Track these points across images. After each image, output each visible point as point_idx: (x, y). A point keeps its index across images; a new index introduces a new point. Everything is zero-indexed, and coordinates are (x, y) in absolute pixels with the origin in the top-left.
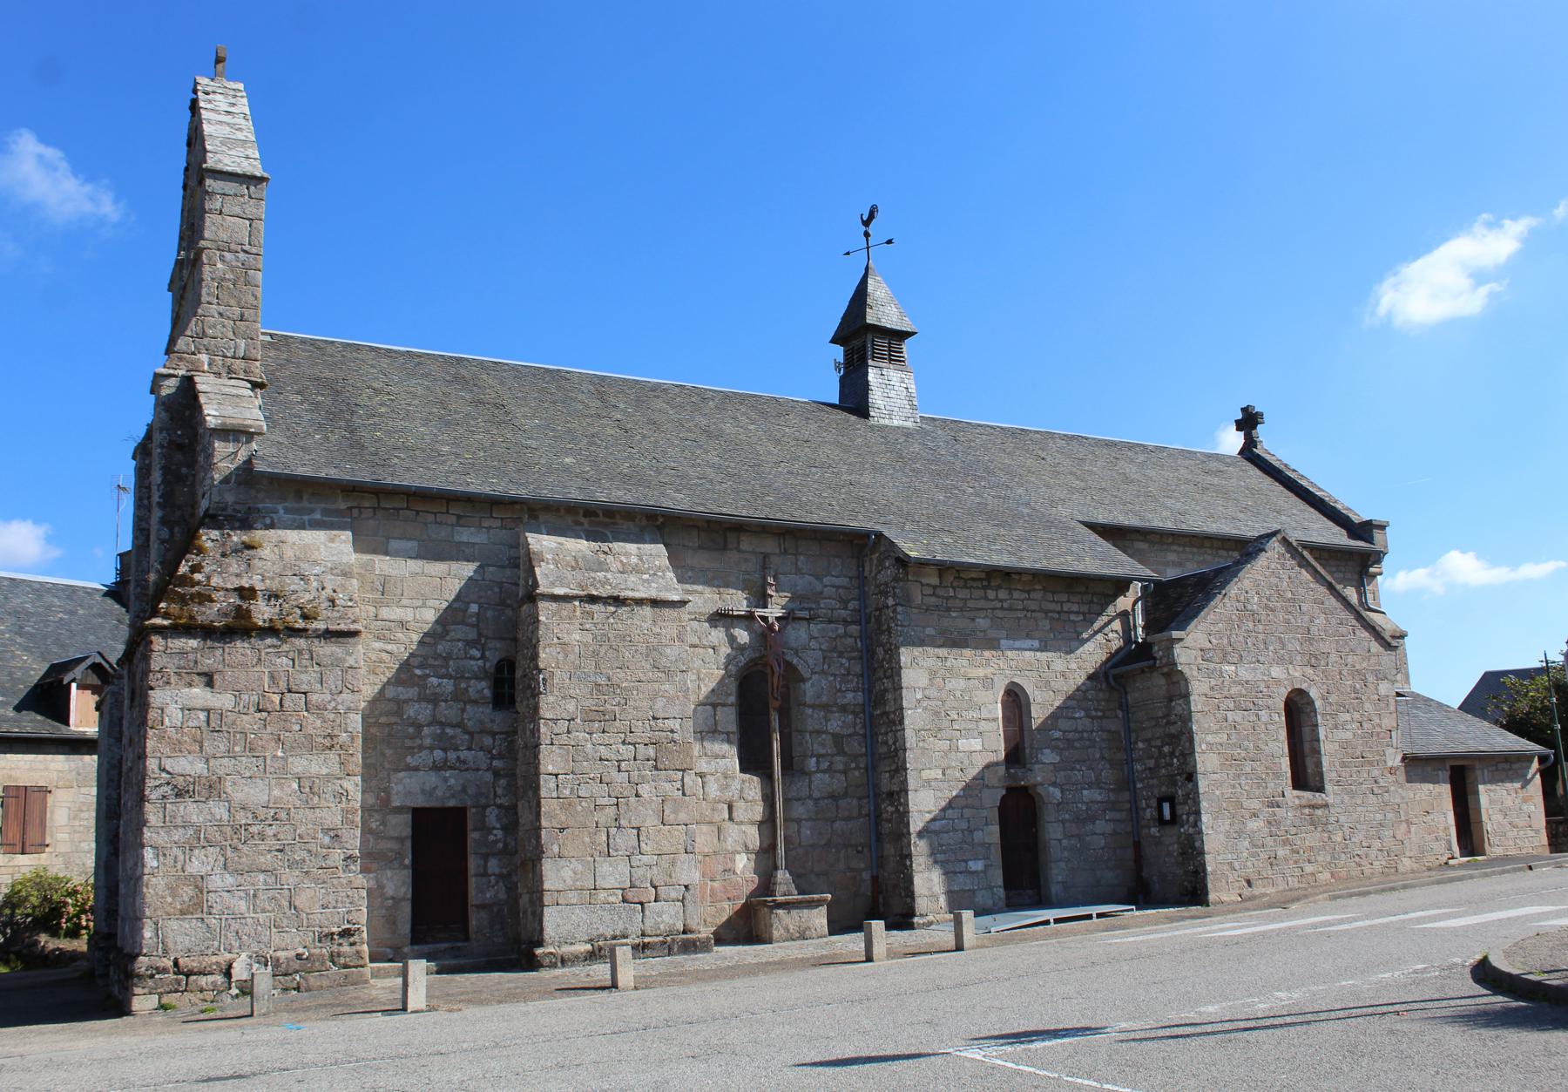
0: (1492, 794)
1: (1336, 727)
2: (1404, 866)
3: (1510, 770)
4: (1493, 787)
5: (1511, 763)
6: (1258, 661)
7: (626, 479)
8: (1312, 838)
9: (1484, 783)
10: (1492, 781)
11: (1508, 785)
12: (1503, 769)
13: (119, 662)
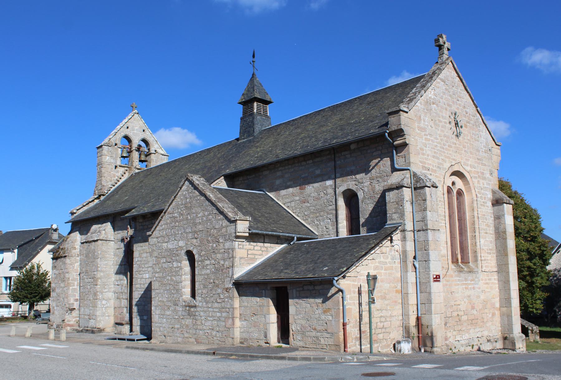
0: (298, 306)
1: (203, 268)
2: (229, 342)
3: (313, 290)
4: (300, 301)
5: (314, 285)
6: (175, 240)
7: (81, 335)
8: (189, 321)
9: (293, 298)
10: (299, 297)
11: (312, 300)
12: (308, 290)
13: (527, 350)
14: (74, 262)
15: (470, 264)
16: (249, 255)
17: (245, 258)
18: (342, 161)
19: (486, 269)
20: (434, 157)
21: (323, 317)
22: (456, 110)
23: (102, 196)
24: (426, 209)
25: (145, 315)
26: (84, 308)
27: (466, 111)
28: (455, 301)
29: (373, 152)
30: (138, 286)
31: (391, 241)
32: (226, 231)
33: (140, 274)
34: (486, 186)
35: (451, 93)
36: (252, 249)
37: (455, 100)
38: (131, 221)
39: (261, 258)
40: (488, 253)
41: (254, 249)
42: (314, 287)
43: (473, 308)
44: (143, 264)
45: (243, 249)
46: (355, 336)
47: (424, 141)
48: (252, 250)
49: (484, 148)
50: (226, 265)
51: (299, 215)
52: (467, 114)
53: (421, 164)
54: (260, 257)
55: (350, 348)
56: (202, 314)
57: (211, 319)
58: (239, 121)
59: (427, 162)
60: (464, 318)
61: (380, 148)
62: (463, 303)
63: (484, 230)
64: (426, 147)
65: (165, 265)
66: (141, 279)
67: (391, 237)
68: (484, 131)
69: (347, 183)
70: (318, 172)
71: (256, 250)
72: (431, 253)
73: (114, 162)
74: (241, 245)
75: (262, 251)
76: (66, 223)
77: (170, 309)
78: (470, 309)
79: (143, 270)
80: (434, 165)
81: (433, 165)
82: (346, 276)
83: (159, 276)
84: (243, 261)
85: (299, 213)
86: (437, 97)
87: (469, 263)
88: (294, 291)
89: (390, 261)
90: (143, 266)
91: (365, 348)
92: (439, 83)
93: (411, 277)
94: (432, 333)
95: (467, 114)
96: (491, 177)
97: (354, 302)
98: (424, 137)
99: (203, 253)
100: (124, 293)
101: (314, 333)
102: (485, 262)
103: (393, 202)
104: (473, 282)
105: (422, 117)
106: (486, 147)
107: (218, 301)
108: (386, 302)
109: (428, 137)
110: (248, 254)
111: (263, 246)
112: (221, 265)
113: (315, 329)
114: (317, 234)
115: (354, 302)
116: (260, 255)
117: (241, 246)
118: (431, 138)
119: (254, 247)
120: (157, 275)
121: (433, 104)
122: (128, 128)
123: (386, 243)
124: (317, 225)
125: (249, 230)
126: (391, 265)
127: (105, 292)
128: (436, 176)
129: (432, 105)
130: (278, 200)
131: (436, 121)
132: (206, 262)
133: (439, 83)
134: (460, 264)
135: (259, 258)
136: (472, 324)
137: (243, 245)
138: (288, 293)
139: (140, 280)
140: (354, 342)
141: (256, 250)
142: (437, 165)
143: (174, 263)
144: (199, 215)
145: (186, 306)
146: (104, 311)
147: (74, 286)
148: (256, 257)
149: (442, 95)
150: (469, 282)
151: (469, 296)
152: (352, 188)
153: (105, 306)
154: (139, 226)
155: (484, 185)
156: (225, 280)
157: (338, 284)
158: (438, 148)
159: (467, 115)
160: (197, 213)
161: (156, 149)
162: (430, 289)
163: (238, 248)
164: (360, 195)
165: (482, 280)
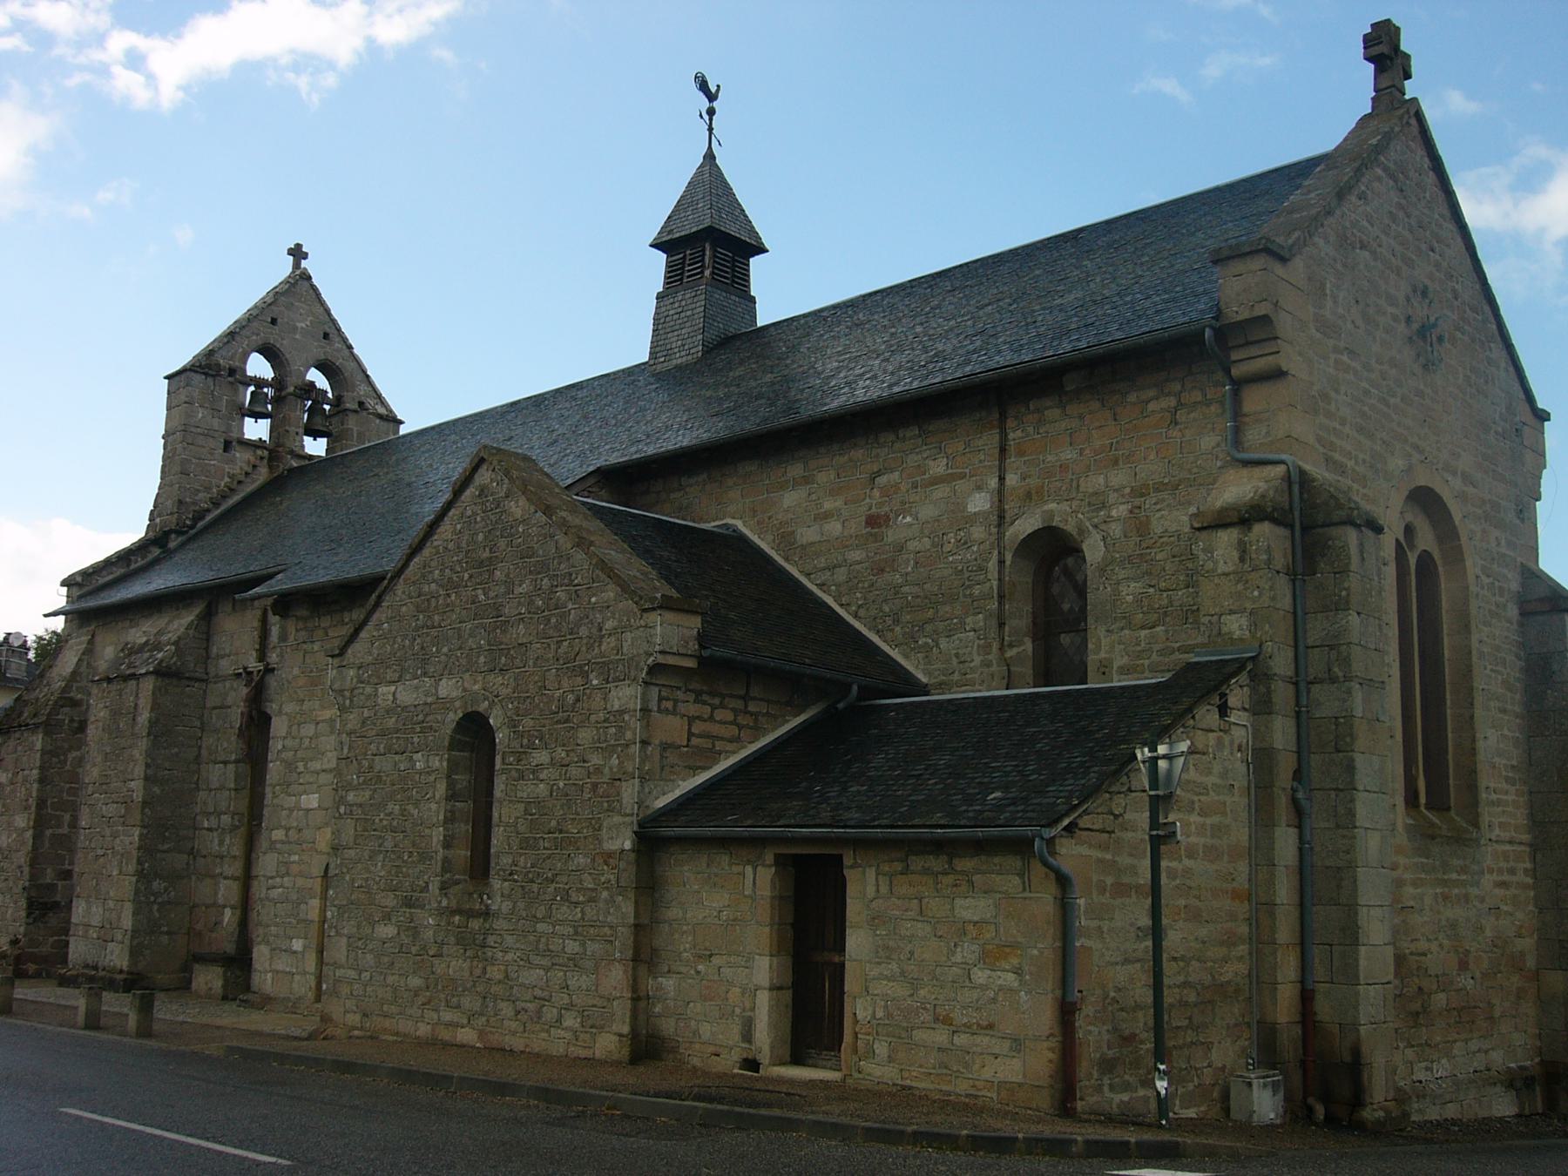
3: (945, 873)
8: (456, 966)
12: (926, 871)
14: (66, 746)
15: (1452, 813)
16: (693, 738)
17: (680, 747)
18: (1030, 429)
19: (1502, 834)
20: (1360, 430)
21: (980, 976)
22: (1427, 282)
23: (173, 536)
24: (1347, 602)
25: (298, 938)
26: (88, 902)
27: (1454, 291)
28: (1412, 941)
29: (1147, 402)
30: (278, 835)
31: (1223, 710)
32: (619, 650)
33: (290, 795)
34: (1503, 550)
35: (1413, 222)
36: (706, 716)
37: (1424, 247)
38: (270, 613)
39: (734, 752)
40: (1507, 779)
41: (711, 718)
42: (950, 863)
43: (1463, 966)
44: (303, 760)
45: (674, 713)
46: (1098, 1055)
47: (1331, 370)
48: (705, 721)
49: (1502, 423)
50: (611, 768)
51: (862, 613)
52: (1456, 299)
53: (1321, 449)
54: (730, 747)
55: (1082, 1099)
56: (509, 940)
57: (545, 962)
58: (652, 304)
59: (1338, 442)
60: (1440, 1000)
61: (1177, 387)
62: (1434, 947)
63: (1497, 699)
64: (1337, 391)
65: (383, 764)
66: (291, 810)
67: (1223, 696)
68: (1503, 365)
69: (1046, 508)
70: (938, 467)
71: (720, 722)
72: (1360, 761)
73: (223, 429)
74: (668, 699)
75: (741, 727)
76: (45, 616)
77: (393, 921)
78: (1455, 973)
79: (301, 781)
80: (1361, 456)
81: (1356, 457)
82: (1077, 824)
83: (359, 800)
84: (672, 758)
85: (860, 607)
86: (1372, 226)
87: (1448, 809)
88: (871, 874)
89: (1218, 781)
90: (301, 769)
91: (1131, 1099)
92: (1379, 179)
93: (1285, 842)
94: (1356, 1052)
95: (1456, 299)
96: (1518, 522)
97: (1099, 927)
98: (1333, 357)
99: (528, 722)
100: (226, 860)
101: (940, 1037)
102: (1500, 809)
103: (1226, 574)
104: (1464, 877)
105: (1328, 285)
106: (1506, 421)
107: (574, 899)
108: (1203, 932)
109: (1345, 358)
110: (690, 734)
111: (743, 708)
112: (591, 770)
113: (947, 1021)
114: (924, 680)
115: (1099, 927)
116: (731, 741)
117: (669, 705)
118: (1353, 364)
119: (712, 712)
120: (351, 797)
121: (1361, 248)
122: (274, 322)
123: (1207, 715)
124: (927, 649)
125: (702, 647)
126: (1221, 798)
127: (164, 852)
128: (1365, 495)
129: (1358, 251)
130: (787, 559)
131: (1368, 305)
132: (535, 754)
133: (1379, 179)
134: (1422, 809)
135: (727, 752)
136: (1460, 1022)
137: (676, 701)
138: (844, 877)
139: (289, 816)
140: (1095, 1077)
141: (720, 722)
142: (1368, 458)
143: (415, 756)
144: (518, 590)
145: (454, 912)
146: (157, 915)
147: (59, 826)
148: (719, 745)
149: (1387, 222)
150: (1454, 876)
151: (1453, 925)
152: (1061, 525)
153: (160, 900)
154: (297, 630)
155: (1499, 544)
156: (605, 824)
157: (1053, 853)
158: (1372, 401)
159: (1456, 303)
160: (510, 585)
161: (363, 399)
162: (1355, 890)
163: (659, 711)
164: (1093, 550)
165: (1491, 871)
